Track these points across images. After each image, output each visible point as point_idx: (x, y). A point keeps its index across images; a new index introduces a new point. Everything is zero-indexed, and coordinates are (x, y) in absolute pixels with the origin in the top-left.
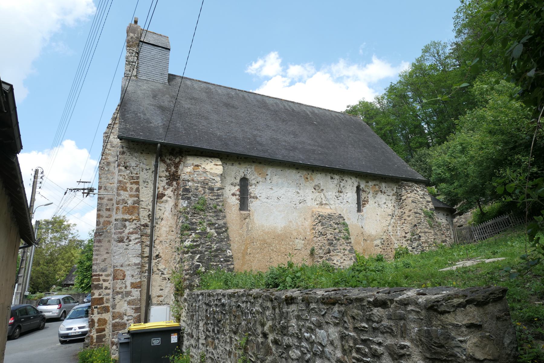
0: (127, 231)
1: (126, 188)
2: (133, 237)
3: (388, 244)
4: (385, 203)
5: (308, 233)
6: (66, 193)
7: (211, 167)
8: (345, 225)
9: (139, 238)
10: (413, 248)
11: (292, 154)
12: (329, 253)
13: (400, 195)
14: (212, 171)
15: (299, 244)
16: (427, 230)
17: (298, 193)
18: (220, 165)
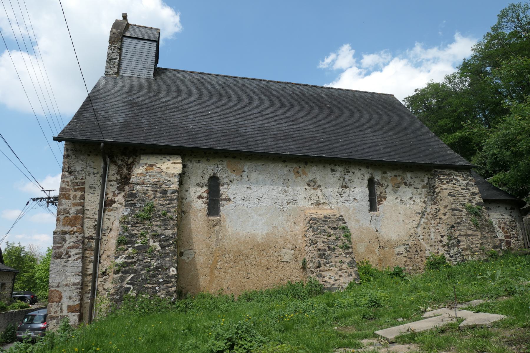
0: (66, 245)
1: (69, 195)
2: (73, 252)
3: (417, 251)
4: (411, 198)
5: (299, 241)
6: (28, 203)
7: (168, 166)
8: (345, 229)
9: (79, 253)
10: (451, 257)
11: (280, 144)
12: (319, 267)
13: (433, 187)
14: (169, 171)
15: (287, 254)
16: (470, 232)
17: (286, 191)
18: (179, 163)
